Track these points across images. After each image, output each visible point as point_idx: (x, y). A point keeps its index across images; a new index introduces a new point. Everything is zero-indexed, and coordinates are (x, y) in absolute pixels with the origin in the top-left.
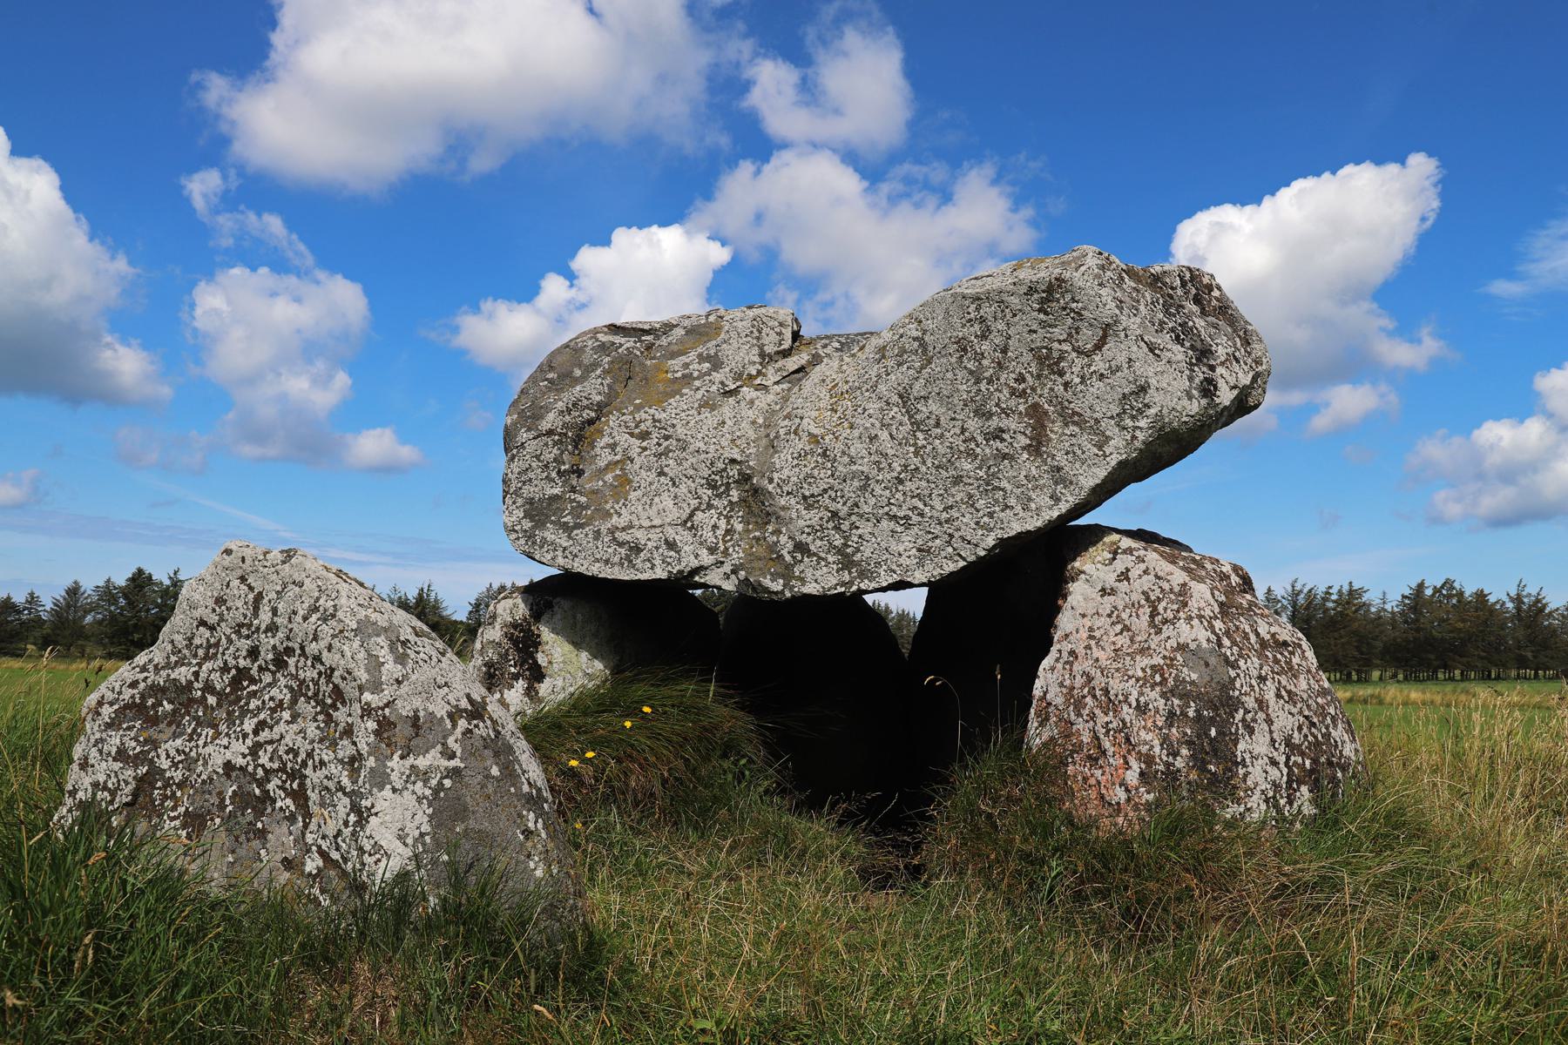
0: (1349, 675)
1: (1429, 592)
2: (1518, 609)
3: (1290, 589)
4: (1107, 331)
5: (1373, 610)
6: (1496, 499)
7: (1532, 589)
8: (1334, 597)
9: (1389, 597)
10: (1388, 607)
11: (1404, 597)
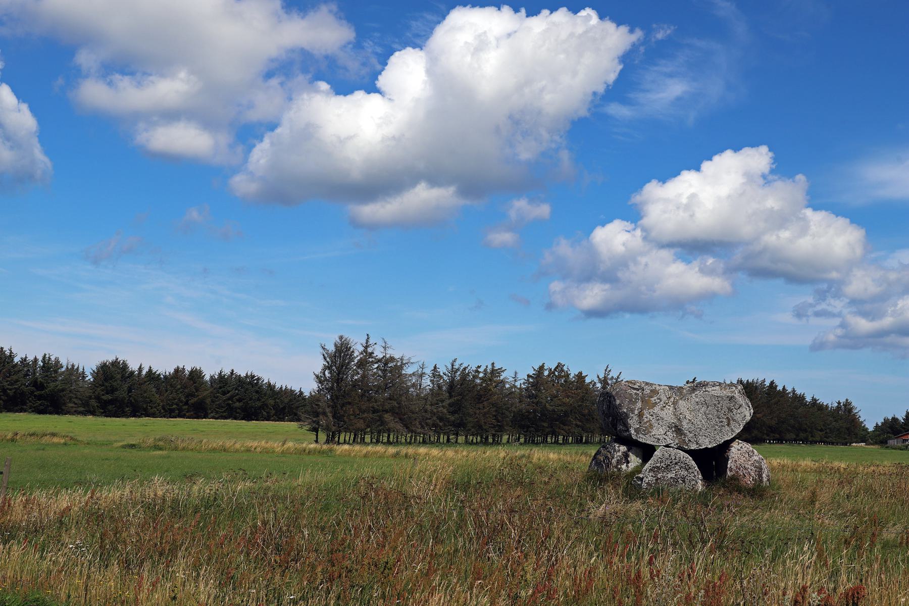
0: (487, 438)
1: (546, 373)
2: (604, 388)
3: (450, 367)
4: (741, 406)
5: (507, 386)
6: (593, 295)
7: (614, 374)
8: (481, 375)
9: (519, 376)
10: (518, 384)
11: (529, 376)
